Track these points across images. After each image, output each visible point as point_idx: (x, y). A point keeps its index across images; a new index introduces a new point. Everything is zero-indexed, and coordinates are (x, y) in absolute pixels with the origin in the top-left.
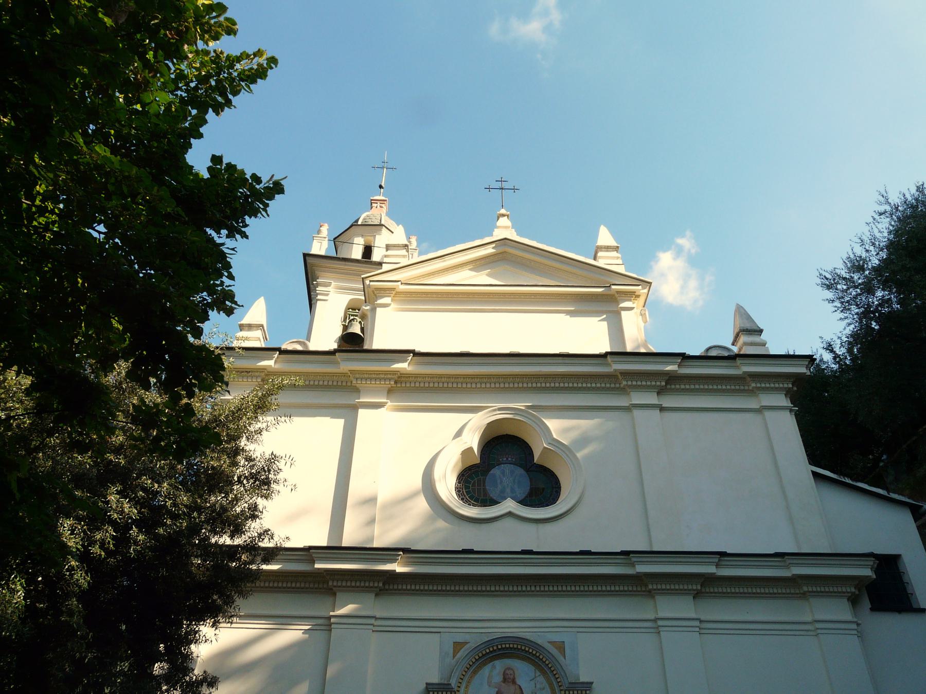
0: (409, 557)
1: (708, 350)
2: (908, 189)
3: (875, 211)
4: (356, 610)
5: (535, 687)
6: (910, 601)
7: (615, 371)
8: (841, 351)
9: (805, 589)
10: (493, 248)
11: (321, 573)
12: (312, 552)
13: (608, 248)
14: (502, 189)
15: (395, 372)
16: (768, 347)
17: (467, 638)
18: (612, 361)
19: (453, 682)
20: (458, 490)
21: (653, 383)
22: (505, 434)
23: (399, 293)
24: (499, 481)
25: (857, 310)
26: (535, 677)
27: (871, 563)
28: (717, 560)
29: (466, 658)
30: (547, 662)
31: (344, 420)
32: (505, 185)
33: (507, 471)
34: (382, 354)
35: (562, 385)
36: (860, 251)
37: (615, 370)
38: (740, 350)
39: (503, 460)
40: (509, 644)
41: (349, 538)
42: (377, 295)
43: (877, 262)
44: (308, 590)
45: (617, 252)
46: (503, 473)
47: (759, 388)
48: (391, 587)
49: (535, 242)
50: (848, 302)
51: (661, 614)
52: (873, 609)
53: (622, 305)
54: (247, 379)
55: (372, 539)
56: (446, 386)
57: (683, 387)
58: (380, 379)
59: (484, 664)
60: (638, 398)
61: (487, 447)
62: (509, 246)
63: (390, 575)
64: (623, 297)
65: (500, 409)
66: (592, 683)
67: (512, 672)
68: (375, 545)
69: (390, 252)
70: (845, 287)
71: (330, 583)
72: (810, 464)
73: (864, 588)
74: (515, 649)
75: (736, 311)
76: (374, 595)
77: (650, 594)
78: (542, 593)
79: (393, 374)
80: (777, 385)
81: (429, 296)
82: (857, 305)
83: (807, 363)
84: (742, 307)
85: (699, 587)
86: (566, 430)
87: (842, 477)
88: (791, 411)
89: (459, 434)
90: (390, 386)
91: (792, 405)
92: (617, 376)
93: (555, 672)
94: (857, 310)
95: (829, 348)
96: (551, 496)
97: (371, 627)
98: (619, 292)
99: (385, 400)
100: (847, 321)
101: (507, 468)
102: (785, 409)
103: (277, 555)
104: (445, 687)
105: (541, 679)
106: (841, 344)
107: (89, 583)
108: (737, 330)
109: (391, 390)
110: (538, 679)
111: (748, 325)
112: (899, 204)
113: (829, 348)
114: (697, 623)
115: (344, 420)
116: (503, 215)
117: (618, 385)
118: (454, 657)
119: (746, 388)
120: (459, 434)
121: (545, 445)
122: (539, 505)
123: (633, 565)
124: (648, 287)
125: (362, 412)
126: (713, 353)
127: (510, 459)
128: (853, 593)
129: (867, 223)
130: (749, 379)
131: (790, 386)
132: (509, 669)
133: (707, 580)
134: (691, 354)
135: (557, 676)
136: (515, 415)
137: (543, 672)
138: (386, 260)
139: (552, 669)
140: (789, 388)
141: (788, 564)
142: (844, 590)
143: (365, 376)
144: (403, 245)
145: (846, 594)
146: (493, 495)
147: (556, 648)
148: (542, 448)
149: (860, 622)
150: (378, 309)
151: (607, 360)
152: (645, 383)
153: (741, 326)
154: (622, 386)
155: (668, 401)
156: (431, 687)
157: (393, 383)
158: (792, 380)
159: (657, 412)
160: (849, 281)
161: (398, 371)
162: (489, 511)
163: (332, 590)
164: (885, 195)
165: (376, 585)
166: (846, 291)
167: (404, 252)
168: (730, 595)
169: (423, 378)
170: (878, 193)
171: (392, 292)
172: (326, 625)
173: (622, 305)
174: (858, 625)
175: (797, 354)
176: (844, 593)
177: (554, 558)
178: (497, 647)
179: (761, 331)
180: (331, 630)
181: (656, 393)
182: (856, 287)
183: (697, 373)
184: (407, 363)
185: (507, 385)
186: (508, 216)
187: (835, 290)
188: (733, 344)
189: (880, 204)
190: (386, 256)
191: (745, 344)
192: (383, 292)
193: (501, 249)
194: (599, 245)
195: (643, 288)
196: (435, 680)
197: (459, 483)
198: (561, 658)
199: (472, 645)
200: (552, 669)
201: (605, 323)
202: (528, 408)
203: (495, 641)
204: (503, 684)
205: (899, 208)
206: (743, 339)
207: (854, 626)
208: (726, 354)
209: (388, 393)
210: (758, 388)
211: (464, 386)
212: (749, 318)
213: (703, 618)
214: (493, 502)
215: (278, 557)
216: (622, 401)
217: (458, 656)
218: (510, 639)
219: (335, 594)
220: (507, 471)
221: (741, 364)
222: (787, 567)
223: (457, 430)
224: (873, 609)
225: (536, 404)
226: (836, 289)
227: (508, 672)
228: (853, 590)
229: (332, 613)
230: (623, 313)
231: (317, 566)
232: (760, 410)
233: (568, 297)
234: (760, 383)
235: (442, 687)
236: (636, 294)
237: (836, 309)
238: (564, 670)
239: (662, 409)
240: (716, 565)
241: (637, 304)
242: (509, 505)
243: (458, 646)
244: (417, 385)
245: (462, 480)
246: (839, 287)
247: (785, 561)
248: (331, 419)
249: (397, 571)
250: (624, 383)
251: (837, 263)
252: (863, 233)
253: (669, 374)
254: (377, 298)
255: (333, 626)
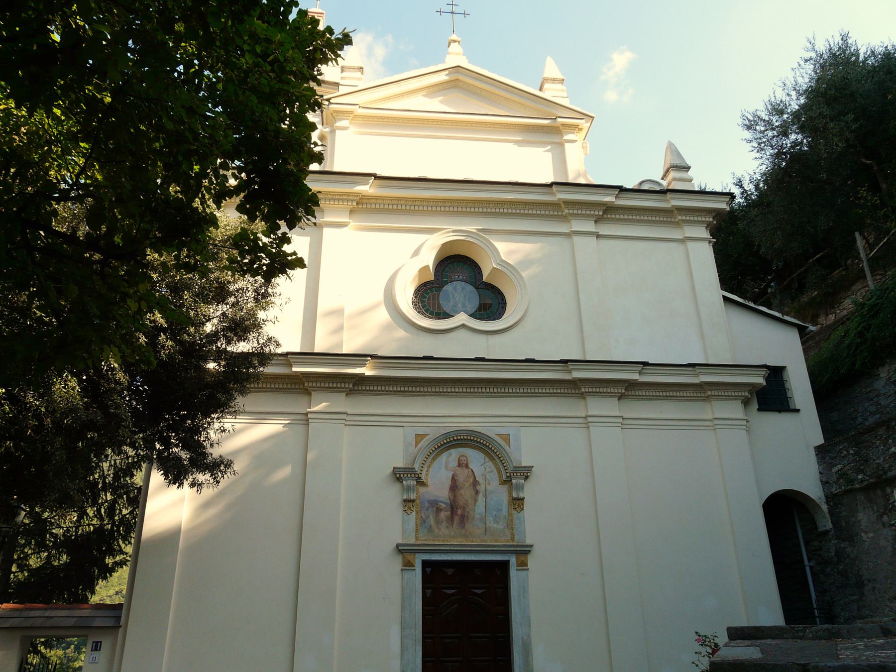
0: (376, 362)
1: (641, 183)
2: (833, 36)
3: (801, 58)
4: (328, 406)
5: (485, 470)
6: (788, 403)
7: (559, 201)
8: (749, 187)
9: (709, 393)
10: (447, 75)
11: (297, 376)
12: (290, 357)
13: (554, 80)
14: (453, 13)
15: (357, 194)
16: (694, 183)
17: (427, 431)
18: (557, 191)
19: (417, 467)
20: (415, 304)
21: (592, 212)
22: (457, 254)
23: (355, 116)
24: (451, 296)
25: (771, 151)
26: (485, 463)
27: (764, 373)
28: (640, 369)
29: (427, 448)
30: (495, 451)
31: (309, 238)
32: (456, 9)
33: (459, 288)
34: (341, 176)
35: (510, 211)
36: (781, 95)
37: (559, 199)
38: (669, 184)
39: (455, 278)
40: (464, 436)
41: (320, 346)
42: (336, 117)
43: (797, 107)
44: (442, 394)
45: (562, 84)
46: (455, 289)
47: (684, 220)
48: (360, 388)
49: (487, 71)
50: (764, 142)
51: (590, 413)
52: (760, 409)
53: (567, 137)
54: (330, 202)
55: (340, 345)
56: (396, 208)
57: (618, 217)
58: (343, 200)
59: (442, 452)
60: (578, 225)
61: (440, 265)
62: (461, 73)
63: (359, 378)
64: (567, 129)
65: (454, 231)
66: (533, 467)
67: (465, 459)
68: (344, 352)
69: (345, 74)
70: (763, 129)
71: (306, 384)
72: (722, 289)
73: (755, 393)
74: (469, 440)
75: (668, 147)
76: (345, 394)
77: (583, 396)
78: (518, 395)
79: (355, 196)
80: (700, 219)
81: (386, 120)
82: (772, 146)
83: (728, 200)
84: (673, 144)
85: (623, 391)
86: (511, 253)
87: (747, 301)
88: (710, 242)
89: (416, 253)
90: (352, 206)
91: (711, 237)
92: (560, 204)
93: (502, 459)
94: (771, 151)
95: (739, 184)
96: (497, 311)
97: (344, 421)
98: (563, 125)
99: (347, 220)
100: (761, 161)
101: (459, 285)
102: (704, 240)
103: (271, 360)
104: (410, 470)
105: (490, 464)
106: (750, 180)
107: (128, 381)
108: (668, 166)
109: (354, 211)
110: (487, 464)
111: (677, 162)
112: (824, 52)
113: (739, 184)
114: (620, 420)
115: (309, 238)
116: (455, 41)
117: (560, 213)
118: (416, 447)
119: (673, 220)
120: (416, 253)
121: (494, 266)
122: (487, 318)
123: (570, 372)
124: (590, 121)
125: (326, 231)
126: (646, 187)
127: (461, 277)
128: (746, 397)
129: (792, 69)
130: (676, 212)
131: (711, 220)
132: (463, 456)
133: (631, 385)
134: (628, 187)
135: (503, 462)
136: (468, 237)
137: (492, 459)
138: (341, 82)
139: (500, 456)
140: (710, 222)
141: (697, 372)
142: (740, 394)
143: (351, 198)
144: (358, 67)
145: (741, 398)
146: (447, 308)
147: (503, 440)
148: (492, 268)
149: (749, 419)
150: (337, 132)
151: (553, 190)
152: (561, 213)
153: (672, 162)
154: (564, 214)
155: (605, 229)
156: (398, 470)
157: (355, 204)
158: (713, 215)
159: (593, 239)
160: (769, 124)
161: (360, 193)
162: (443, 323)
163: (308, 390)
164: (813, 42)
165: (347, 386)
166: (763, 132)
167: (358, 74)
168: (685, 398)
169: (383, 200)
170: (806, 40)
171: (351, 115)
172: (305, 419)
173: (567, 137)
174: (747, 421)
175: (707, 190)
176: (739, 396)
177: (522, 365)
178: (453, 438)
179: (689, 168)
180: (588, 427)
181: (594, 221)
182: (773, 129)
183: (579, 198)
184: (369, 186)
185: (460, 209)
186: (459, 42)
187: (753, 131)
188: (662, 179)
189: (807, 50)
190: (342, 78)
191: (674, 179)
192: (341, 115)
193: (454, 77)
194: (546, 77)
195: (587, 122)
196: (400, 464)
197: (416, 297)
198: (507, 448)
199: (432, 437)
200: (500, 456)
201: (550, 154)
202: (479, 231)
203: (452, 433)
204: (457, 468)
205: (824, 55)
206: (673, 174)
207: (745, 423)
208: (658, 188)
209: (350, 213)
210: (684, 221)
211: (421, 208)
212: (679, 155)
213: (625, 416)
214: (447, 316)
215: (272, 362)
216: (563, 228)
217: (420, 445)
218: (465, 432)
219: (310, 394)
220: (459, 288)
221: (671, 198)
222: (697, 375)
223: (414, 250)
224: (760, 409)
225: (487, 228)
226: (755, 130)
227: (462, 458)
228: (747, 394)
229: (309, 410)
230: (567, 145)
231: (294, 369)
232: (683, 241)
233: (517, 128)
234: (686, 216)
235: (407, 470)
236: (579, 127)
237: (753, 149)
238: (509, 456)
239: (598, 236)
240: (639, 373)
241: (578, 136)
242: (461, 318)
243: (419, 437)
244: (378, 206)
245: (418, 295)
246: (758, 128)
247: (568, 366)
248: (298, 237)
249: (366, 374)
250: (567, 211)
251: (759, 106)
252: (787, 78)
253: (606, 204)
254: (335, 120)
255: (310, 421)
